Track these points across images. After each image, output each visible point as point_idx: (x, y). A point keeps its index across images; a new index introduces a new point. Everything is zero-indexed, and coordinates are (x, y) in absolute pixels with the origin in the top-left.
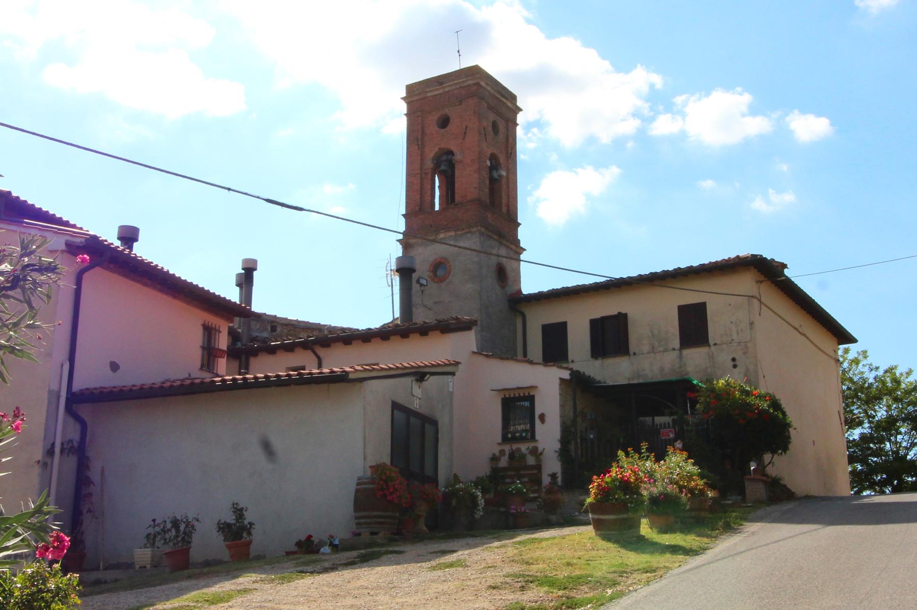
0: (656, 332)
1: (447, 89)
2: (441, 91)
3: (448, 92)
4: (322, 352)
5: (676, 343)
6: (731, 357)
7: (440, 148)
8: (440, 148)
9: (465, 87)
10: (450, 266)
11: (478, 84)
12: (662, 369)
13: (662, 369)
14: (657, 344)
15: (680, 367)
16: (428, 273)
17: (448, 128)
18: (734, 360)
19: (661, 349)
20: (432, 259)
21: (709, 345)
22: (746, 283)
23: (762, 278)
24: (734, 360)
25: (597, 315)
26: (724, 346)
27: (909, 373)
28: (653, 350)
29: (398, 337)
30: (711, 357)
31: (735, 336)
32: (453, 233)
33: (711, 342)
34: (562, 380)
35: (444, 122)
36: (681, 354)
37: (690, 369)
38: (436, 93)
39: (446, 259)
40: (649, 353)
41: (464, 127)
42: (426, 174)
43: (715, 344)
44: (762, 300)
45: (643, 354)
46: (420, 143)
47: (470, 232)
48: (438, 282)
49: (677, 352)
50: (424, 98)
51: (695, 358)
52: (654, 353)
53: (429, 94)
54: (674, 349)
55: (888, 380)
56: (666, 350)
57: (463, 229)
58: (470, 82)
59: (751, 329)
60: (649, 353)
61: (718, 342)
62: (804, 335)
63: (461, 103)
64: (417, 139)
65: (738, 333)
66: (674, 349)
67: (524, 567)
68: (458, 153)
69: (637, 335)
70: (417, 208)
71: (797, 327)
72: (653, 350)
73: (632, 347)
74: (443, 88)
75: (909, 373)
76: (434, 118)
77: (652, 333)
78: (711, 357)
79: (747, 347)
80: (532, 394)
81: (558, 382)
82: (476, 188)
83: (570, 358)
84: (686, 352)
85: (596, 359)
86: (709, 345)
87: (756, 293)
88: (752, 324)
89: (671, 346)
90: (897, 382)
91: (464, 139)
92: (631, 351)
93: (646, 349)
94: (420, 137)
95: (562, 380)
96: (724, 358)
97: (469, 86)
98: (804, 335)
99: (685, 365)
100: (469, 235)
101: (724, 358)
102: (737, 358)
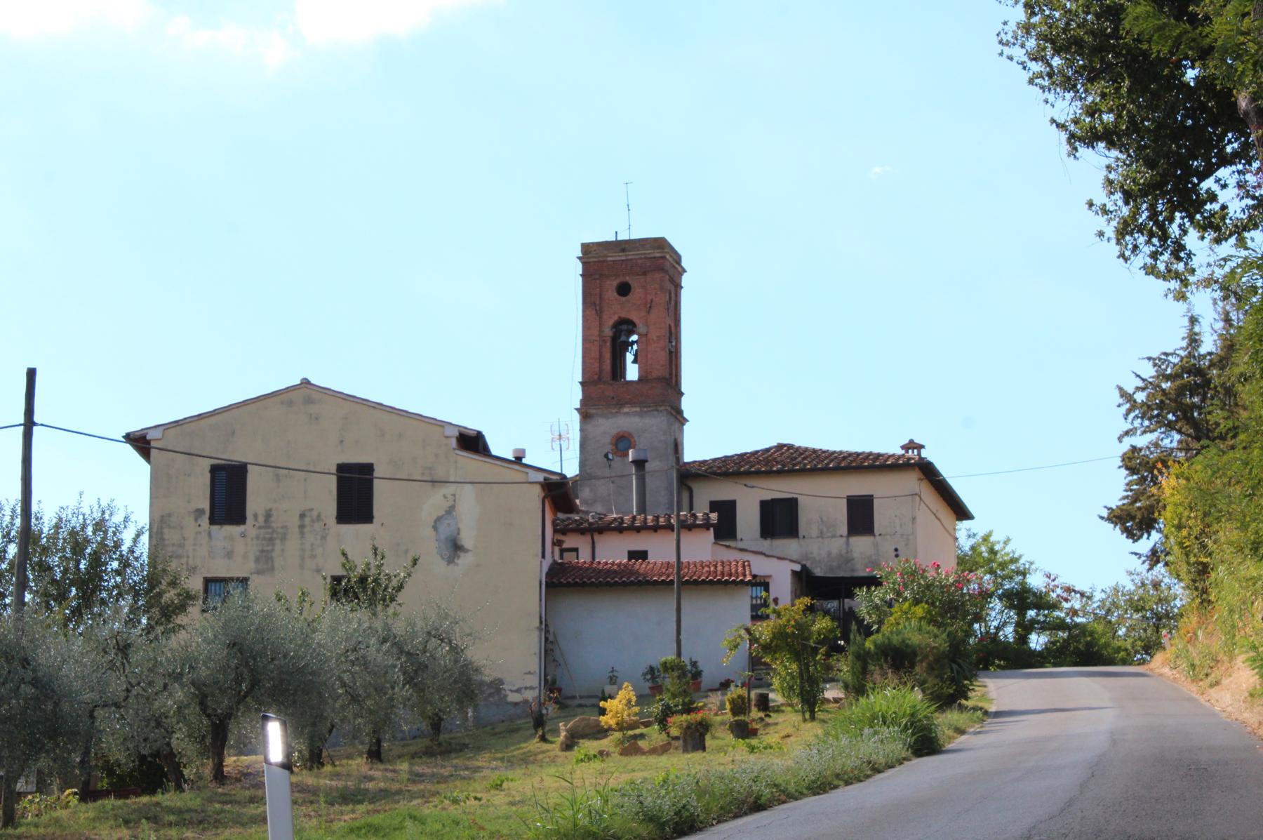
0: (824, 519)
1: (629, 257)
2: (623, 258)
3: (631, 260)
4: (596, 537)
5: (844, 529)
6: (894, 547)
7: (620, 317)
8: (620, 317)
9: (651, 258)
10: (635, 441)
11: (664, 258)
12: (829, 554)
13: (829, 554)
14: (825, 530)
15: (847, 552)
16: (610, 446)
17: (628, 297)
18: (896, 550)
19: (830, 535)
20: (614, 432)
21: (874, 535)
22: (912, 481)
23: (923, 477)
24: (896, 550)
25: (768, 496)
26: (888, 537)
27: (1007, 542)
28: (821, 535)
29: (686, 531)
30: (876, 546)
31: (898, 528)
32: (638, 409)
33: (877, 531)
34: (794, 572)
35: (624, 290)
36: (848, 543)
37: (855, 555)
38: (618, 258)
39: (630, 435)
40: (818, 537)
41: (649, 301)
42: (604, 341)
43: (880, 535)
44: (922, 496)
45: (811, 538)
46: (598, 308)
47: (658, 411)
48: (621, 456)
49: (844, 539)
50: (604, 261)
51: (861, 545)
52: (823, 538)
53: (609, 259)
54: (841, 536)
55: (983, 549)
56: (833, 536)
57: (650, 407)
58: (658, 255)
59: (913, 523)
60: (818, 537)
61: (883, 533)
62: (939, 519)
63: (645, 273)
64: (595, 304)
65: (901, 525)
66: (841, 536)
67: (376, 819)
68: (641, 325)
69: (806, 517)
70: (596, 377)
71: (935, 512)
72: (821, 535)
73: (801, 532)
74: (626, 255)
75: (1007, 542)
76: (613, 284)
77: (822, 519)
78: (876, 546)
79: (908, 539)
80: (767, 580)
81: (790, 572)
82: (662, 366)
83: (739, 536)
84: (853, 540)
85: (766, 539)
86: (874, 535)
87: (918, 491)
88: (914, 519)
89: (839, 533)
90: (992, 552)
91: (649, 312)
92: (801, 533)
93: (815, 533)
94: (598, 302)
95: (794, 572)
96: (887, 547)
97: (655, 258)
98: (939, 519)
99: (851, 551)
100: (656, 413)
101: (887, 547)
102: (898, 548)
